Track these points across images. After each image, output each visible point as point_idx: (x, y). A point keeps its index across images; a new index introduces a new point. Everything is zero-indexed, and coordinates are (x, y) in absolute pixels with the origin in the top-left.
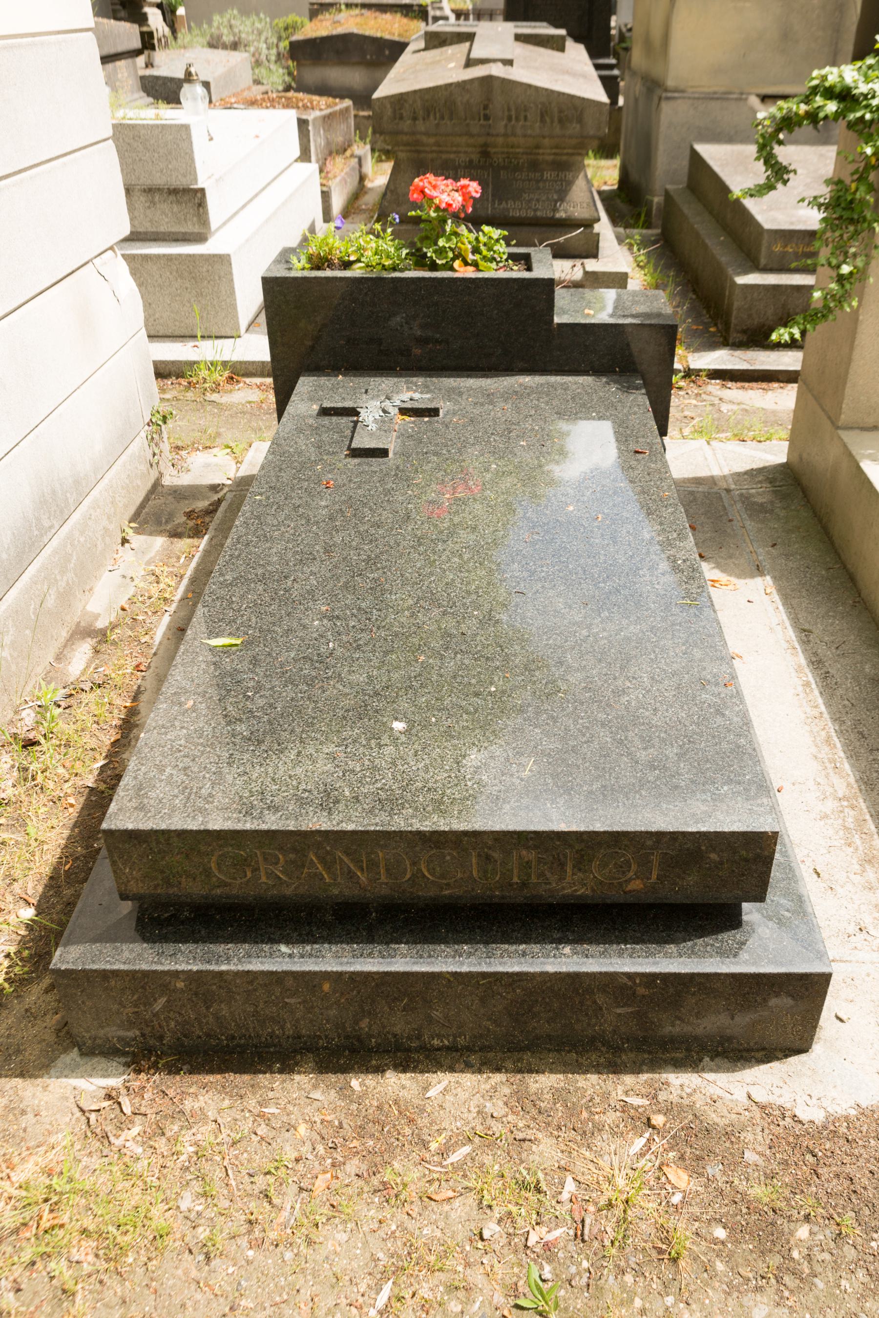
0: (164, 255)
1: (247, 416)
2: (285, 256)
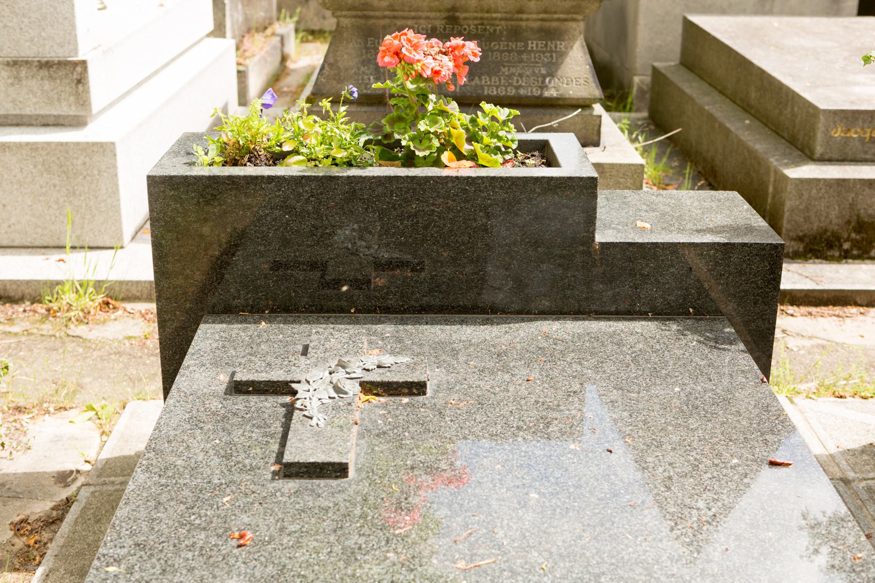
0: (27, 144)
1: (124, 359)
2: (185, 146)
